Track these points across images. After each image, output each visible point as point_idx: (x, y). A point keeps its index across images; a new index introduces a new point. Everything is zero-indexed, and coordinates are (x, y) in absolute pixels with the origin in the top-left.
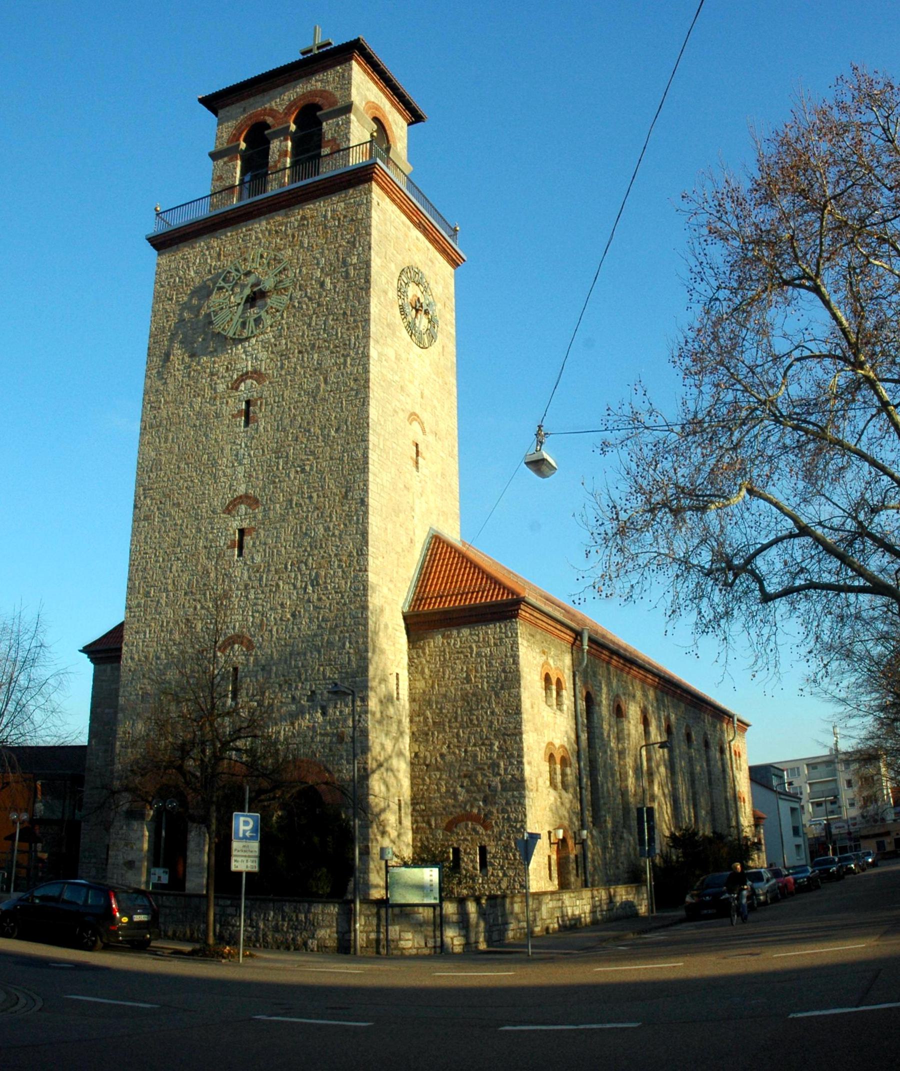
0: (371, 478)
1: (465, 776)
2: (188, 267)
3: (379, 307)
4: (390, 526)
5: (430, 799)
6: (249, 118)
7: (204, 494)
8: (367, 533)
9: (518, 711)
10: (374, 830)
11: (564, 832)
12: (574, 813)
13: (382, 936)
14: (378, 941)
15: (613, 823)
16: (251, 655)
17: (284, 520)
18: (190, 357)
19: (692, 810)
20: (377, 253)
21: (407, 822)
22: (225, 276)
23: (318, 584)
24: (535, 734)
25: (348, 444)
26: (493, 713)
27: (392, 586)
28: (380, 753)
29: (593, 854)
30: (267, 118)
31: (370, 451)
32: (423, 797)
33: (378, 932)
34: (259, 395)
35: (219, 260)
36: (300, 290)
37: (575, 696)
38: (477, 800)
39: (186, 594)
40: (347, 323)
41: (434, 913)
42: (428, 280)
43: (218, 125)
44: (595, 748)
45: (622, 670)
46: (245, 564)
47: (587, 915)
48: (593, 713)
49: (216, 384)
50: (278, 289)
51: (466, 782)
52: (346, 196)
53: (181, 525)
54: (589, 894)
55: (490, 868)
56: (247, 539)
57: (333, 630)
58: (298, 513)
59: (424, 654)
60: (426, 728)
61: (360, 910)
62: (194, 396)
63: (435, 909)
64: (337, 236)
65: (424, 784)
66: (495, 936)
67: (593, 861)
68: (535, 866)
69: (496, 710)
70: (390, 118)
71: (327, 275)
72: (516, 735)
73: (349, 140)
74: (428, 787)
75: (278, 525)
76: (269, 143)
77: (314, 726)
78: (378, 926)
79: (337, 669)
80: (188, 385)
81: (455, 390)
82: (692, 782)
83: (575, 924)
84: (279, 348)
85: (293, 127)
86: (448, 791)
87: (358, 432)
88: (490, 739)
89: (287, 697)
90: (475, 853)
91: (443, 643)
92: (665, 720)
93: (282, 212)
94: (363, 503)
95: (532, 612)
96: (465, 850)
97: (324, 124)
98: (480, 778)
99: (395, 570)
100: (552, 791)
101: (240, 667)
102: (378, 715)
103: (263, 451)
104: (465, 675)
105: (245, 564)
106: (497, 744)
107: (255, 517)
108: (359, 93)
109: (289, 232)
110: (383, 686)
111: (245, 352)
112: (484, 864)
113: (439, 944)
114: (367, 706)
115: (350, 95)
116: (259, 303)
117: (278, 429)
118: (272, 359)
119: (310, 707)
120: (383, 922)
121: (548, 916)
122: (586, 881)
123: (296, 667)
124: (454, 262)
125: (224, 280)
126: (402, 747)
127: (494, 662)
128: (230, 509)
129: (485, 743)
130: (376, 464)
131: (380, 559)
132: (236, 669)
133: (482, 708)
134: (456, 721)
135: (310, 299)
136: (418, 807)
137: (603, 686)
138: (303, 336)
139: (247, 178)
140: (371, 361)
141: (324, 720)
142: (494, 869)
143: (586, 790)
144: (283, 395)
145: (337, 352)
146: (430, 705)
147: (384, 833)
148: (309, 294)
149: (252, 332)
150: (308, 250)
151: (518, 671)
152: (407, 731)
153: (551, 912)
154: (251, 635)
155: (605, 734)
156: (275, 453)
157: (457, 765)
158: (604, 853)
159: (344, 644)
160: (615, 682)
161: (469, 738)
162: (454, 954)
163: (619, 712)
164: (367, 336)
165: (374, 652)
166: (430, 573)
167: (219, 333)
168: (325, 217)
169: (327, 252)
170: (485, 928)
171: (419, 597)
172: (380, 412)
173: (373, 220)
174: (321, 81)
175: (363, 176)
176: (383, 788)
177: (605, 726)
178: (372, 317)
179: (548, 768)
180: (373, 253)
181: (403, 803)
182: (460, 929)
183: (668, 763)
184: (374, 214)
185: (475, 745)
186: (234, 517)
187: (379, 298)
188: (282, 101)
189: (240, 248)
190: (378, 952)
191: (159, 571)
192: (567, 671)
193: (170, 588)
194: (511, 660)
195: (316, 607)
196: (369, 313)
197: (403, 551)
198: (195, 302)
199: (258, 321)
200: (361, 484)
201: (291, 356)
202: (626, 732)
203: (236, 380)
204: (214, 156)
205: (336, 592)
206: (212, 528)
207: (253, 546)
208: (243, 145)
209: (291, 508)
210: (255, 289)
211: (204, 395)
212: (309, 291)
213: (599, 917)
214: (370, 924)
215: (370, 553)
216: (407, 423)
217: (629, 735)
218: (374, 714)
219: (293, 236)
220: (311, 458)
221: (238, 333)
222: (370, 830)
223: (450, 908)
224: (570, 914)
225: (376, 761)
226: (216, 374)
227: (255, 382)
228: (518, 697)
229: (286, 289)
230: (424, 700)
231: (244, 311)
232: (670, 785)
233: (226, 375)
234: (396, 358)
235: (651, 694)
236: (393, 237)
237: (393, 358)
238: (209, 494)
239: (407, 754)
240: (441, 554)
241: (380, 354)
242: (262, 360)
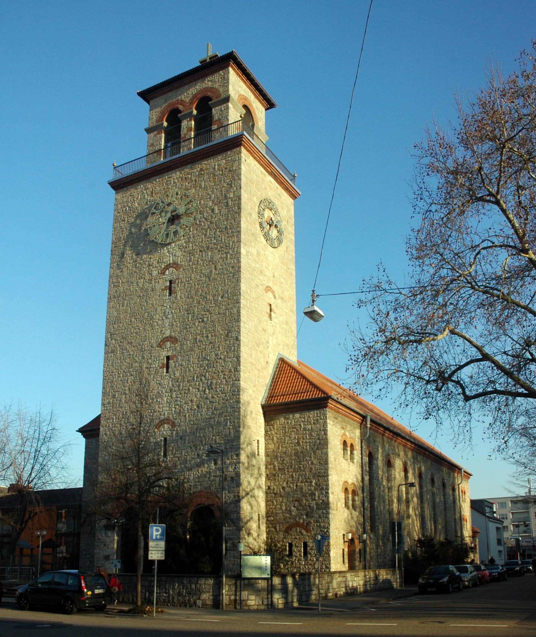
0: (242, 324)
1: (296, 500)
2: (134, 201)
3: (246, 223)
4: (253, 352)
5: (276, 513)
6: (169, 106)
7: (146, 336)
8: (240, 357)
9: (326, 463)
10: (243, 533)
11: (353, 535)
12: (359, 524)
13: (238, 598)
14: (235, 600)
15: (383, 530)
16: (174, 430)
17: (192, 350)
18: (136, 255)
19: (433, 525)
20: (245, 191)
21: (263, 527)
22: (156, 206)
23: (212, 389)
24: (336, 476)
25: (229, 305)
26: (312, 463)
27: (255, 389)
28: (247, 487)
29: (370, 549)
30: (179, 106)
31: (241, 309)
32: (272, 513)
33: (236, 595)
34: (177, 277)
35: (152, 196)
36: (200, 214)
37: (362, 454)
38: (302, 514)
39: (136, 395)
40: (227, 233)
41: (268, 583)
42: (277, 207)
43: (150, 110)
44: (373, 485)
45: (392, 439)
46: (170, 377)
47: (361, 587)
48: (373, 465)
49: (151, 271)
50: (187, 213)
51: (296, 504)
52: (226, 156)
53: (133, 355)
54: (363, 574)
55: (309, 556)
56: (171, 362)
57: (220, 415)
58: (200, 346)
59: (274, 428)
60: (274, 472)
61: (226, 581)
62: (139, 279)
63: (268, 581)
64: (221, 181)
65: (273, 505)
66: (304, 598)
67: (370, 553)
68: (334, 555)
69: (314, 462)
70: (254, 106)
71: (216, 205)
72: (325, 476)
73: (228, 120)
74: (276, 506)
75: (189, 353)
76: (181, 123)
77: (210, 471)
78: (236, 591)
79: (223, 438)
80: (135, 272)
81: (294, 272)
82: (434, 507)
83: (354, 592)
84: (188, 249)
85: (195, 112)
86: (286, 509)
87: (235, 298)
88: (310, 479)
89: (195, 455)
90: (301, 547)
91: (284, 422)
92: (418, 469)
93: (189, 166)
94: (238, 339)
95: (336, 405)
96: (295, 544)
97: (213, 110)
98: (304, 502)
99: (257, 380)
100: (346, 510)
101: (168, 437)
102: (246, 465)
103: (180, 310)
104: (296, 441)
105: (170, 377)
106: (314, 481)
107: (175, 349)
108: (234, 89)
109: (193, 178)
110: (249, 447)
111: (168, 252)
112: (306, 553)
113: (270, 603)
114: (240, 459)
115: (228, 90)
116: (176, 222)
117: (188, 297)
118: (184, 256)
119: (207, 460)
120: (239, 589)
121: (337, 587)
122: (365, 565)
123: (200, 437)
124: (294, 196)
125: (155, 208)
126: (261, 483)
127: (313, 433)
128: (161, 345)
129: (307, 481)
130: (245, 316)
131: (248, 374)
132: (165, 439)
133: (306, 460)
134: (291, 468)
135: (206, 219)
136: (269, 519)
137: (380, 448)
138: (202, 241)
139: (169, 145)
140: (242, 256)
141: (216, 468)
142: (311, 556)
143: (367, 510)
144: (191, 277)
145: (222, 250)
146: (277, 459)
147: (249, 534)
148: (205, 217)
149: (172, 240)
150: (204, 189)
151: (327, 439)
152: (264, 474)
153: (339, 584)
154: (174, 419)
155: (380, 477)
156: (187, 311)
157: (292, 494)
158: (377, 548)
159: (227, 423)
160: (387, 446)
161: (299, 478)
162: (278, 609)
163: (389, 464)
164: (239, 241)
165: (244, 427)
166: (278, 382)
167: (153, 241)
168: (214, 169)
169: (215, 190)
170: (298, 593)
171: (271, 396)
172: (248, 286)
173: (242, 170)
174: (211, 81)
175: (236, 143)
176: (249, 507)
177: (380, 472)
178: (242, 230)
179: (344, 497)
180: (242, 191)
181: (261, 516)
182: (282, 593)
183: (419, 496)
184: (243, 167)
185: (302, 482)
186: (163, 349)
187: (246, 218)
188: (188, 94)
189: (164, 189)
190: (235, 608)
191: (121, 382)
192: (357, 439)
193: (127, 392)
194: (323, 433)
195: (211, 402)
196: (240, 227)
197: (262, 369)
198: (138, 222)
199: (176, 233)
200: (236, 328)
201: (195, 253)
202: (393, 476)
203: (163, 269)
204: (149, 131)
205: (222, 393)
206: (151, 356)
207: (175, 367)
208: (165, 124)
209: (196, 343)
210: (174, 214)
211: (145, 278)
212: (205, 214)
213: (368, 588)
214: (231, 591)
215: (241, 370)
216: (265, 292)
217: (395, 478)
218: (243, 464)
219: (196, 181)
220: (207, 313)
221: (164, 240)
222: (241, 533)
223: (277, 581)
224: (350, 586)
225: (245, 491)
226: (152, 265)
227: (174, 270)
228: (327, 454)
229: (192, 213)
230: (274, 455)
231: (167, 227)
232: (419, 509)
233: (158, 265)
234: (257, 254)
235: (410, 454)
236: (254, 180)
237: (256, 254)
238: (149, 336)
239: (264, 487)
240: (284, 371)
241: (247, 252)
242: (178, 257)
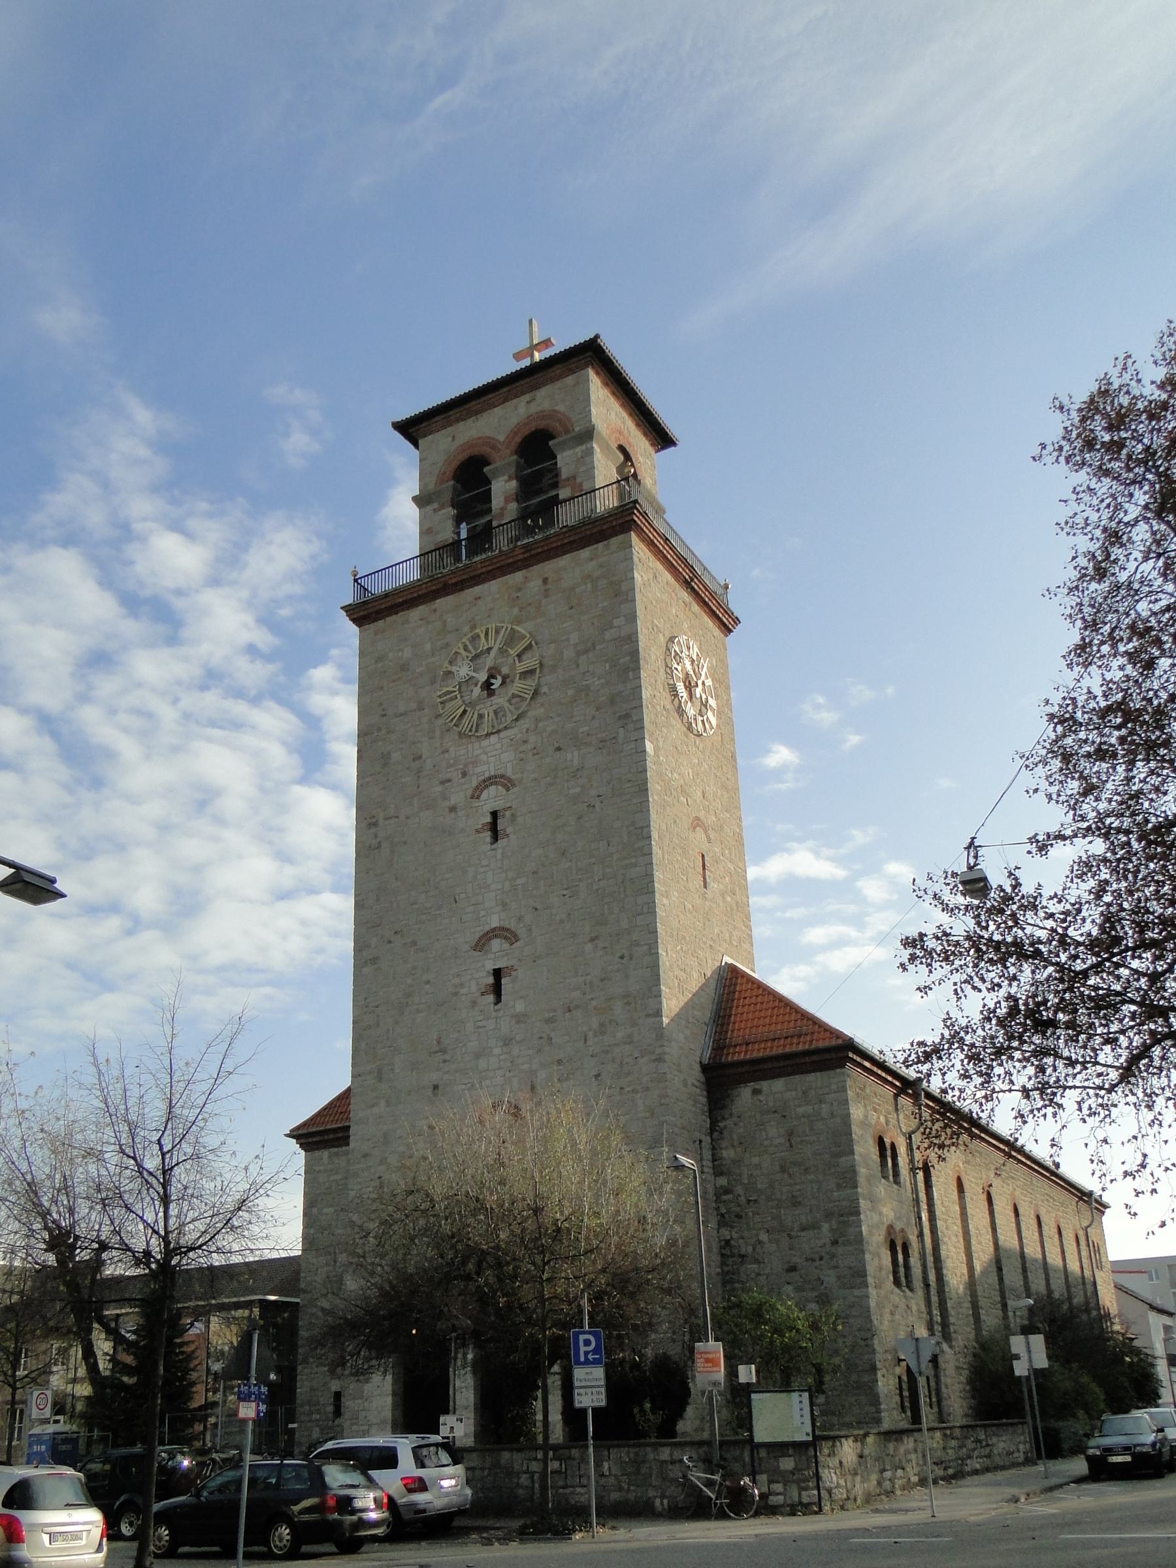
128: (481, 944)
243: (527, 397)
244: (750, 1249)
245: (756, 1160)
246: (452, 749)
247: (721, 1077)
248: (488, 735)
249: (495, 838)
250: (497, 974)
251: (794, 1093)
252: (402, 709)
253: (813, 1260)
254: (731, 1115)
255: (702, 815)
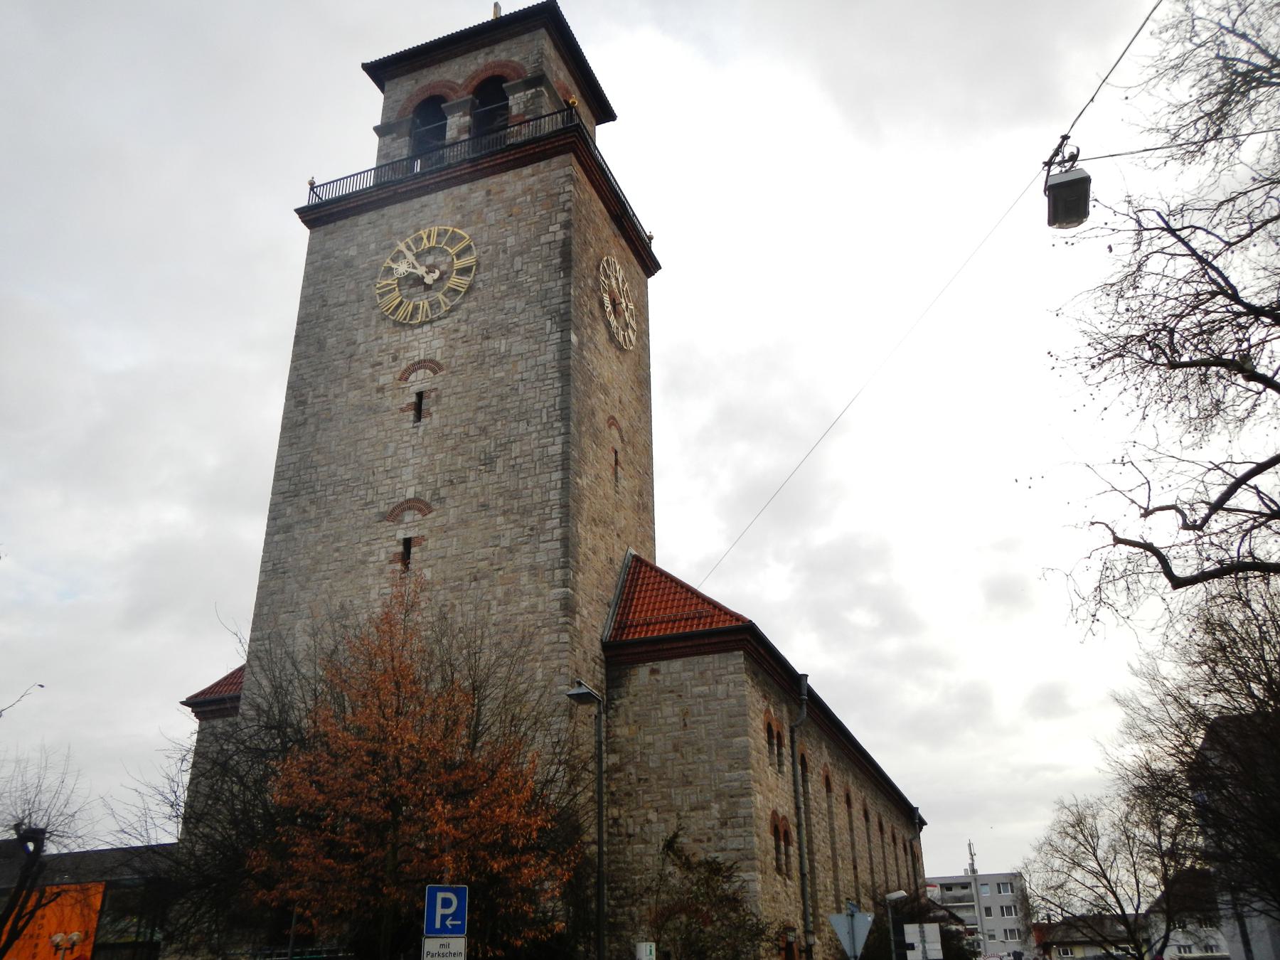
128: (395, 515)
243: (487, 50)
244: (638, 830)
245: (649, 739)
246: (386, 336)
247: (621, 654)
248: (421, 324)
249: (418, 417)
250: (407, 543)
251: (691, 674)
252: (342, 299)
253: (701, 841)
254: (628, 693)
255: (617, 416)
